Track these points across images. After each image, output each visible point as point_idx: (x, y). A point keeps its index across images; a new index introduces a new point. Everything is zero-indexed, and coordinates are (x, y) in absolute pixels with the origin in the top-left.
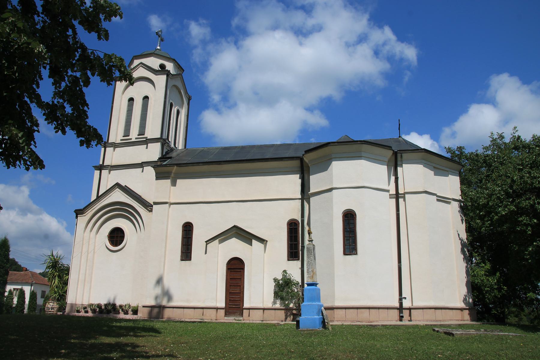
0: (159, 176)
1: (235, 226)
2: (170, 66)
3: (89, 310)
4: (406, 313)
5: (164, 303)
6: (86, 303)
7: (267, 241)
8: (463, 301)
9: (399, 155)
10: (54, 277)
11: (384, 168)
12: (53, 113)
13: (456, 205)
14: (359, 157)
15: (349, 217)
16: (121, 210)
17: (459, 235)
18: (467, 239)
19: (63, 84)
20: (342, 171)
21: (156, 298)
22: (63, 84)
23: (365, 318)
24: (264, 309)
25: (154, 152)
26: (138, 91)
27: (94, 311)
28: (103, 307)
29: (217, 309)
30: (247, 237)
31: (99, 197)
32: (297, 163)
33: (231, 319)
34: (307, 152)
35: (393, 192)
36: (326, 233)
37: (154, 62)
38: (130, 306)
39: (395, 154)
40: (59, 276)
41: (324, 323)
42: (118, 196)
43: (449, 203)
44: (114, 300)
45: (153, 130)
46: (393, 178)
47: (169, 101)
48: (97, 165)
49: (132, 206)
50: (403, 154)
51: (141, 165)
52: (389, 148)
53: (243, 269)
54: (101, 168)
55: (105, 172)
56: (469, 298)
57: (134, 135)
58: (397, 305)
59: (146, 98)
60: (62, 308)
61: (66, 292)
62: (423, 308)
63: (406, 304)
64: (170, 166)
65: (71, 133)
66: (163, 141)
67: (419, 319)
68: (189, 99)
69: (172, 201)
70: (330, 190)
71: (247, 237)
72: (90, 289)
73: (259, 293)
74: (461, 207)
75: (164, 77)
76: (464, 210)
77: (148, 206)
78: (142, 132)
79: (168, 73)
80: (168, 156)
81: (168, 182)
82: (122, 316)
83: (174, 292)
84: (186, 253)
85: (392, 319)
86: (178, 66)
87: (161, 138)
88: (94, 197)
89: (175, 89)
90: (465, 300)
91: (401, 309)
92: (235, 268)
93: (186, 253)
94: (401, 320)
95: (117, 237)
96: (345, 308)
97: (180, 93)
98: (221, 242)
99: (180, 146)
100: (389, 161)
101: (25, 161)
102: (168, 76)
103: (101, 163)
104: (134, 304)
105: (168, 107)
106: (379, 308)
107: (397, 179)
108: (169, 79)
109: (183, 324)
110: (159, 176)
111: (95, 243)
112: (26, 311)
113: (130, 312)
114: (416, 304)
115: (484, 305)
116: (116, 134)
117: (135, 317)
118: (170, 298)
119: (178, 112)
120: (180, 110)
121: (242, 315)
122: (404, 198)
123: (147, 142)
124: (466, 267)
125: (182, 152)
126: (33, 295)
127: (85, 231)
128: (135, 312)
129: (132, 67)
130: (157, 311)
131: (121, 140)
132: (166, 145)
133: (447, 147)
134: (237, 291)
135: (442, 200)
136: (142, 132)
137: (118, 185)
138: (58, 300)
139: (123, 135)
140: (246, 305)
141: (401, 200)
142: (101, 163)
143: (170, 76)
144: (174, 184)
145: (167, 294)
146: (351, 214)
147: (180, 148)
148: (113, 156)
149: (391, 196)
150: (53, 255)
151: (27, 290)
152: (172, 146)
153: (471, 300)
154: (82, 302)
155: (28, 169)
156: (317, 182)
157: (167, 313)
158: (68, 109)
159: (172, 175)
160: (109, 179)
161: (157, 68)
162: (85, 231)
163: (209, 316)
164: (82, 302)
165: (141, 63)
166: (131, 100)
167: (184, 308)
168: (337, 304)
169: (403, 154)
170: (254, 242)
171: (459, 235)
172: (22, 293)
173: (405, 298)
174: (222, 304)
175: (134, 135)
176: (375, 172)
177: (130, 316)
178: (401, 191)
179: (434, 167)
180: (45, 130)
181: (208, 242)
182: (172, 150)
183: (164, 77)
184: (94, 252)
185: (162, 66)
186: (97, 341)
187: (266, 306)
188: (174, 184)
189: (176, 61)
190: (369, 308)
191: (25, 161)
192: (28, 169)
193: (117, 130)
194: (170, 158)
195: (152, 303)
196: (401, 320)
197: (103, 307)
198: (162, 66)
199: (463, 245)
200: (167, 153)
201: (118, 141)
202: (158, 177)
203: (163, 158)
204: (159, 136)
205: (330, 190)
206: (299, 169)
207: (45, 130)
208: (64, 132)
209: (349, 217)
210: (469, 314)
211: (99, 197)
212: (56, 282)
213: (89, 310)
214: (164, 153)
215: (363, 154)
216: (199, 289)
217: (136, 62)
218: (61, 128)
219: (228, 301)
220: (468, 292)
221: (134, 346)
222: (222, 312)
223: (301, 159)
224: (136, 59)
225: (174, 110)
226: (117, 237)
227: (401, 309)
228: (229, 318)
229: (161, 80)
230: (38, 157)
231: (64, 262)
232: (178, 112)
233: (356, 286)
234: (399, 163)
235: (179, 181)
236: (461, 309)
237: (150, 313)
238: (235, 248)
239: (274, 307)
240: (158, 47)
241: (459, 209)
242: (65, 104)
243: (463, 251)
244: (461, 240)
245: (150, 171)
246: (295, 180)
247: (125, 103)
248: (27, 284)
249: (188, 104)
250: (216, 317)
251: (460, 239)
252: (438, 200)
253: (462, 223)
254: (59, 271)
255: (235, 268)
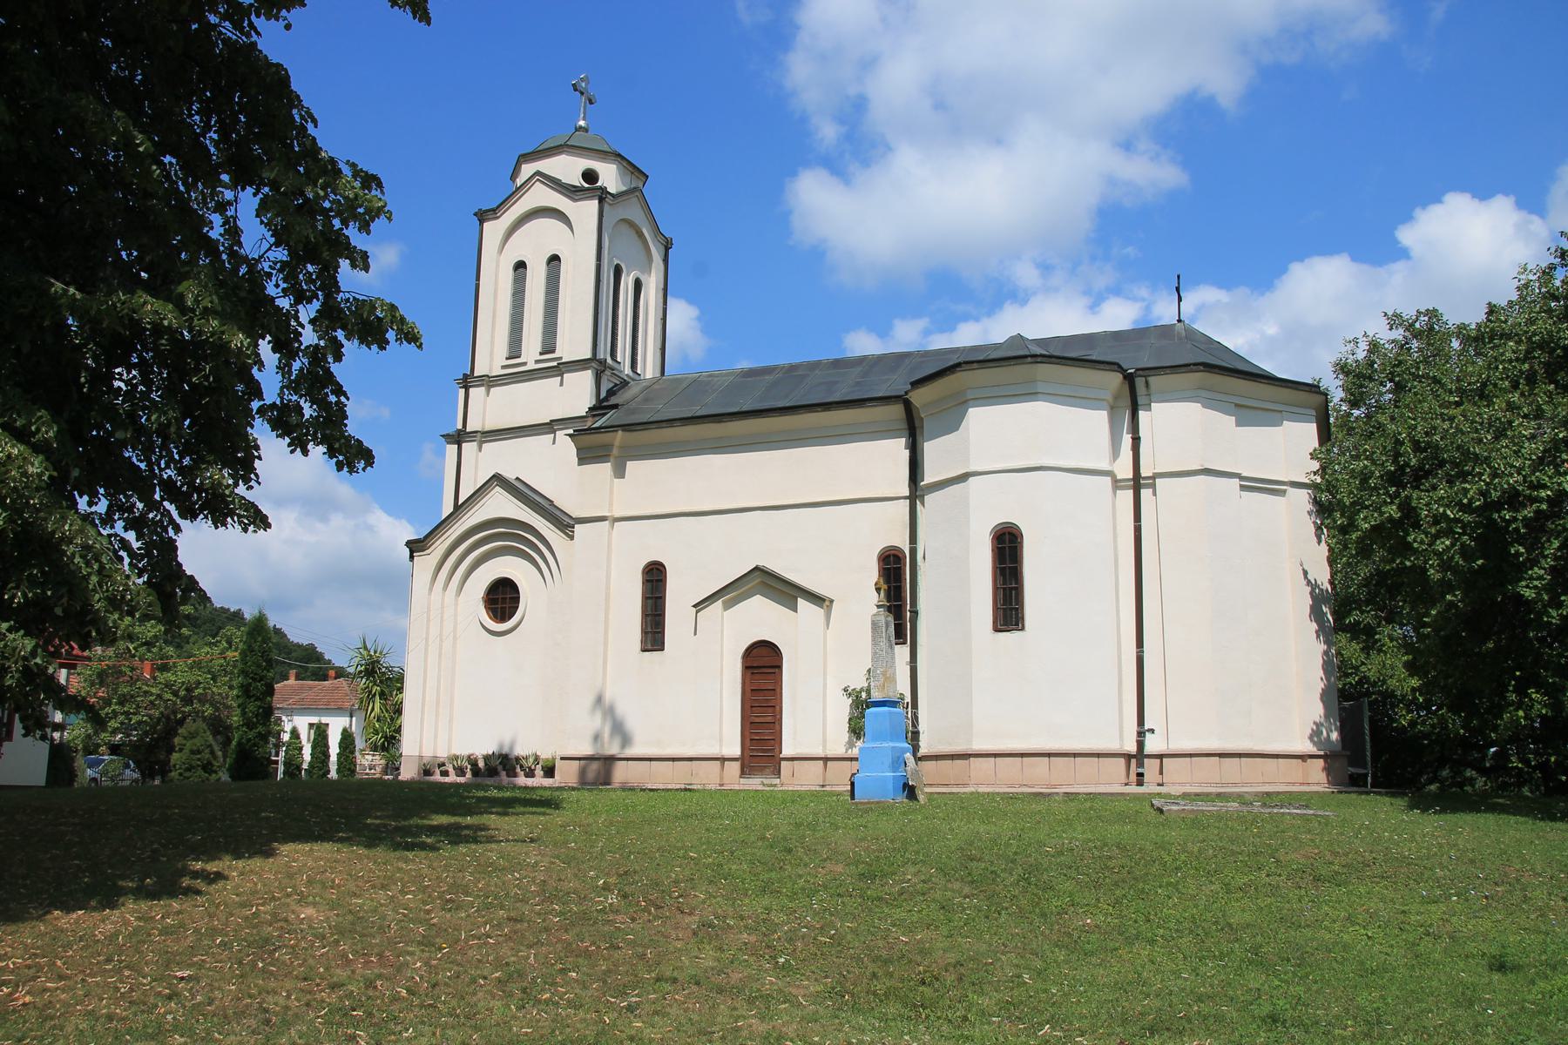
0: (587, 456)
1: (757, 568)
2: (610, 177)
3: (451, 769)
4: (1151, 767)
5: (613, 749)
6: (443, 754)
7: (832, 601)
8: (1311, 738)
9: (1139, 382)
10: (371, 697)
11: (1098, 420)
12: (284, 421)
13: (1303, 498)
14: (1031, 395)
15: (1007, 545)
16: (508, 536)
17: (1305, 573)
18: (1331, 583)
19: (296, 365)
20: (992, 433)
21: (597, 738)
22: (296, 365)
23: (1039, 776)
24: (826, 760)
25: (577, 394)
26: (536, 242)
27: (460, 771)
28: (481, 764)
29: (723, 760)
30: (786, 591)
31: (459, 508)
32: (897, 410)
33: (755, 783)
34: (917, 384)
35: (1124, 470)
36: (956, 584)
37: (568, 168)
38: (537, 759)
39: (1129, 379)
40: (382, 695)
41: (910, 791)
42: (500, 505)
43: (1282, 493)
44: (511, 748)
45: (575, 341)
46: (1127, 440)
47: (610, 261)
48: (451, 431)
49: (533, 526)
50: (1151, 379)
51: (550, 427)
52: (1115, 366)
53: (780, 667)
54: (459, 438)
55: (469, 448)
56: (1329, 731)
57: (531, 354)
58: (1131, 747)
59: (555, 259)
60: (393, 766)
61: (399, 730)
62: (1191, 755)
63: (1153, 745)
64: (618, 425)
65: (317, 451)
66: (598, 366)
67: (1180, 779)
68: (667, 246)
69: (617, 515)
70: (964, 478)
71: (786, 591)
72: (451, 721)
73: (813, 722)
74: (1316, 502)
75: (592, 206)
76: (1322, 509)
77: (565, 524)
78: (549, 347)
79: (603, 196)
80: (613, 401)
81: (606, 468)
82: (522, 780)
83: (633, 724)
84: (654, 634)
85: (1111, 779)
86: (631, 168)
87: (594, 358)
88: (448, 509)
89: (625, 228)
90: (1315, 735)
91: (1140, 756)
92: (762, 663)
93: (654, 634)
94: (1140, 783)
95: (502, 600)
96: (995, 755)
97: (640, 235)
98: (728, 605)
99: (649, 369)
100: (1116, 397)
101: (240, 516)
102: (601, 200)
103: (460, 426)
104: (545, 754)
105: (608, 277)
106: (1075, 755)
107: (1136, 441)
108: (606, 207)
109: (643, 796)
110: (587, 456)
111: (456, 615)
112: (333, 774)
113: (539, 772)
114: (1178, 745)
115: (1375, 747)
116: (491, 356)
117: (548, 782)
118: (626, 740)
119: (638, 285)
120: (643, 278)
121: (778, 773)
122: (1153, 486)
123: (561, 369)
124: (1326, 653)
125: (655, 381)
126: (347, 739)
127: (431, 589)
128: (549, 771)
129: (519, 182)
130: (598, 770)
131: (504, 367)
132: (608, 372)
133: (1390, 313)
134: (769, 719)
135: (1270, 487)
136: (549, 347)
137: (498, 479)
138: (384, 749)
139: (505, 354)
140: (787, 751)
141: (1145, 494)
142: (460, 426)
143: (609, 199)
144: (620, 472)
145: (620, 731)
146: (895, 556)
147: (649, 375)
148: (487, 409)
149: (1117, 484)
150: (365, 648)
151: (336, 726)
152: (627, 370)
153: (1335, 736)
154: (435, 750)
155: (245, 530)
156: (939, 456)
157: (621, 773)
158: (308, 411)
159: (615, 452)
160: (481, 462)
161: (577, 180)
162: (431, 589)
163: (707, 777)
164: (435, 750)
165: (538, 173)
166: (520, 266)
167: (650, 759)
168: (978, 746)
169: (1151, 379)
170: (802, 603)
171: (1305, 573)
172: (320, 733)
173: (1152, 731)
174: (736, 751)
175: (531, 354)
176: (1073, 429)
177: (539, 780)
178: (1145, 472)
179: (1237, 405)
180: (271, 448)
181: (700, 606)
182: (624, 384)
183: (592, 206)
184: (455, 638)
185: (590, 176)
186: (426, 822)
187: (830, 754)
188: (620, 472)
189: (623, 158)
190: (1049, 755)
191: (240, 516)
192: (245, 530)
193: (492, 343)
194: (615, 406)
195: (586, 749)
196: (1140, 783)
197: (481, 764)
198: (590, 176)
199: (1318, 598)
200: (611, 393)
201: (498, 371)
202: (583, 460)
203: (599, 408)
204: (588, 355)
205: (964, 478)
206: (904, 425)
207: (271, 448)
208: (305, 452)
209: (1007, 545)
210: (1324, 769)
211: (459, 508)
212: (377, 709)
213: (451, 769)
214: (603, 395)
215: (1040, 387)
216: (683, 715)
217: (527, 170)
218: (299, 445)
219: (748, 742)
220: (1327, 716)
221: (485, 828)
222: (735, 767)
223: (908, 405)
224: (527, 162)
225: (627, 283)
226: (502, 600)
227: (1140, 756)
228: (750, 781)
229: (585, 212)
230: (258, 511)
231: (389, 661)
232: (638, 285)
233: (1023, 706)
234: (1141, 400)
235: (631, 466)
236: (1303, 757)
237: (583, 772)
238: (760, 618)
239: (850, 753)
240: (582, 123)
241: (1310, 507)
242: (302, 402)
243: (1316, 613)
244: (1313, 586)
245: (564, 445)
246: (895, 450)
247: (507, 275)
248: (338, 710)
249: (666, 260)
250: (721, 778)
251: (1309, 582)
252: (1243, 488)
253: (1319, 542)
254: (381, 683)
255: (762, 663)
